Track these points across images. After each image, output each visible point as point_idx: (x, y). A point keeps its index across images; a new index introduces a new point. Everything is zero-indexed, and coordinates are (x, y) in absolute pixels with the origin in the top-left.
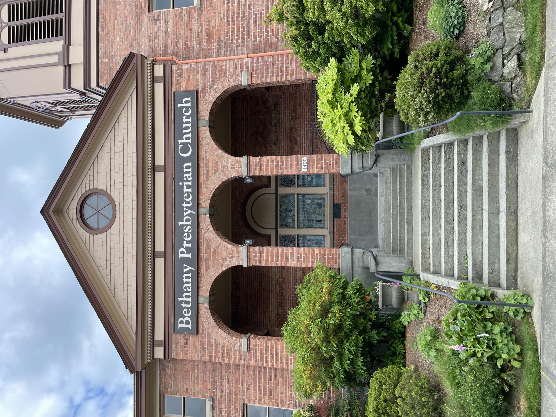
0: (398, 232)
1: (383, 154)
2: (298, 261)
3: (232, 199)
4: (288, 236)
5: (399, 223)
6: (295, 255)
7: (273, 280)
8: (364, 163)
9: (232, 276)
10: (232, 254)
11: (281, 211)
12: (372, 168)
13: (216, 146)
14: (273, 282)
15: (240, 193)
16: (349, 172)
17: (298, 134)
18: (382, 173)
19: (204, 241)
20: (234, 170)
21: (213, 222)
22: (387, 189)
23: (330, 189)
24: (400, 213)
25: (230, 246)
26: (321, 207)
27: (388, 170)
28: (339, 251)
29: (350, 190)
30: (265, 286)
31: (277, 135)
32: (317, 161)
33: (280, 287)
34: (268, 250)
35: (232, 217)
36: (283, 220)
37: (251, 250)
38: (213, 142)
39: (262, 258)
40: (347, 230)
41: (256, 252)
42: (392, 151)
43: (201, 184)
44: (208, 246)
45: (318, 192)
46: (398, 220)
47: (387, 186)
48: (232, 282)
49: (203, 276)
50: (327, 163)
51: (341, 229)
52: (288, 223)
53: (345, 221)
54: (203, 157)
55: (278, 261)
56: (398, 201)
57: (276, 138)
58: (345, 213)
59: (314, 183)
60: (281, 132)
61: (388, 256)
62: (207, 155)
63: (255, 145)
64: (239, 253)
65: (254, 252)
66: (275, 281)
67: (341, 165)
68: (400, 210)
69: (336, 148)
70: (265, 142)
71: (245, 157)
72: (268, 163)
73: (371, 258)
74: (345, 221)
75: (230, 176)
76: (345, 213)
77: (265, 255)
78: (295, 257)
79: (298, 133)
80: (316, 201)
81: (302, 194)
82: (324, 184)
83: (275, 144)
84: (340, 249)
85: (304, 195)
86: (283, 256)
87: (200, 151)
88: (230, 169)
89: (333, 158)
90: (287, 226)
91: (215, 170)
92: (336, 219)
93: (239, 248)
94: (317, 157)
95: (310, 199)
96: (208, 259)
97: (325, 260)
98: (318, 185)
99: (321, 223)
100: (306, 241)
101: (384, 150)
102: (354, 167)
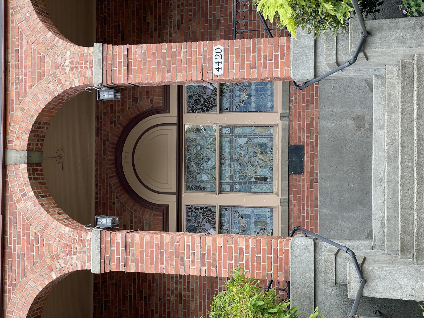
0: (415, 208)
1: (380, 29)
2: (202, 264)
3: (97, 134)
4: (201, 208)
5: (415, 188)
6: (197, 250)
7: (172, 293)
8: (339, 52)
9: (95, 285)
10: (70, 246)
11: (189, 159)
12: (355, 60)
13: (41, 23)
14: (172, 298)
15: (111, 124)
16: (310, 75)
17: (222, 8)
18: (381, 77)
19: (15, 218)
20: (76, 72)
21: (35, 179)
22: (391, 111)
23: (282, 116)
24: (419, 165)
25: (67, 229)
26: (266, 153)
27: (395, 69)
28: (287, 245)
29: (322, 119)
30: (157, 304)
31: (182, 11)
32: (243, 53)
33: (184, 308)
34: (142, 239)
35: (96, 170)
36: (192, 175)
37: (108, 239)
38: (36, 16)
39: (130, 257)
40: (316, 198)
41: (118, 243)
42: (402, 22)
43: (12, 103)
44: (24, 229)
45: (259, 123)
46: (415, 180)
47: (392, 104)
48: (95, 296)
49: (14, 290)
50: (265, 57)
51: (303, 196)
52: (202, 182)
53: (312, 180)
54: (17, 46)
55: (163, 264)
56: (415, 137)
57: (179, 17)
58: (312, 163)
59: (253, 105)
60: (190, 5)
61: (391, 262)
62: (24, 42)
63: (141, 32)
64: (84, 245)
65: (113, 243)
66: (176, 296)
67: (294, 60)
68: (418, 157)
69: (263, 6)
70: (159, 24)
71: (98, 46)
72: (145, 59)
73: (351, 266)
74: (312, 180)
75: (68, 86)
76: (312, 163)
77: (134, 251)
78: (197, 256)
79: (222, 6)
80: (256, 140)
81: (229, 126)
82: (272, 107)
83: (178, 29)
84: (290, 242)
85: (232, 128)
86: (172, 253)
87: (10, 35)
88: (68, 70)
89: (276, 45)
90: (200, 189)
91: (39, 72)
92: (293, 176)
93: (84, 234)
94: (243, 45)
95: (245, 136)
96: (23, 255)
97: (259, 263)
98: (260, 109)
99: (266, 184)
100: (237, 218)
101: (384, 21)
102: (319, 65)
